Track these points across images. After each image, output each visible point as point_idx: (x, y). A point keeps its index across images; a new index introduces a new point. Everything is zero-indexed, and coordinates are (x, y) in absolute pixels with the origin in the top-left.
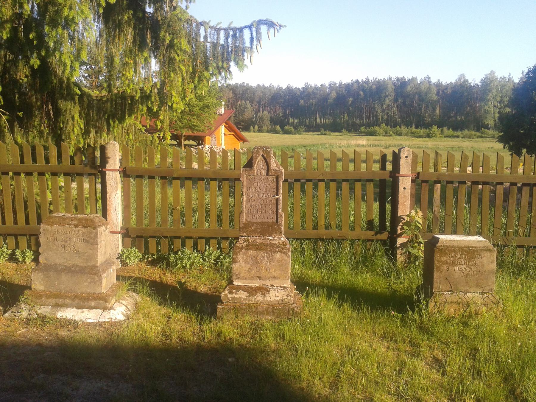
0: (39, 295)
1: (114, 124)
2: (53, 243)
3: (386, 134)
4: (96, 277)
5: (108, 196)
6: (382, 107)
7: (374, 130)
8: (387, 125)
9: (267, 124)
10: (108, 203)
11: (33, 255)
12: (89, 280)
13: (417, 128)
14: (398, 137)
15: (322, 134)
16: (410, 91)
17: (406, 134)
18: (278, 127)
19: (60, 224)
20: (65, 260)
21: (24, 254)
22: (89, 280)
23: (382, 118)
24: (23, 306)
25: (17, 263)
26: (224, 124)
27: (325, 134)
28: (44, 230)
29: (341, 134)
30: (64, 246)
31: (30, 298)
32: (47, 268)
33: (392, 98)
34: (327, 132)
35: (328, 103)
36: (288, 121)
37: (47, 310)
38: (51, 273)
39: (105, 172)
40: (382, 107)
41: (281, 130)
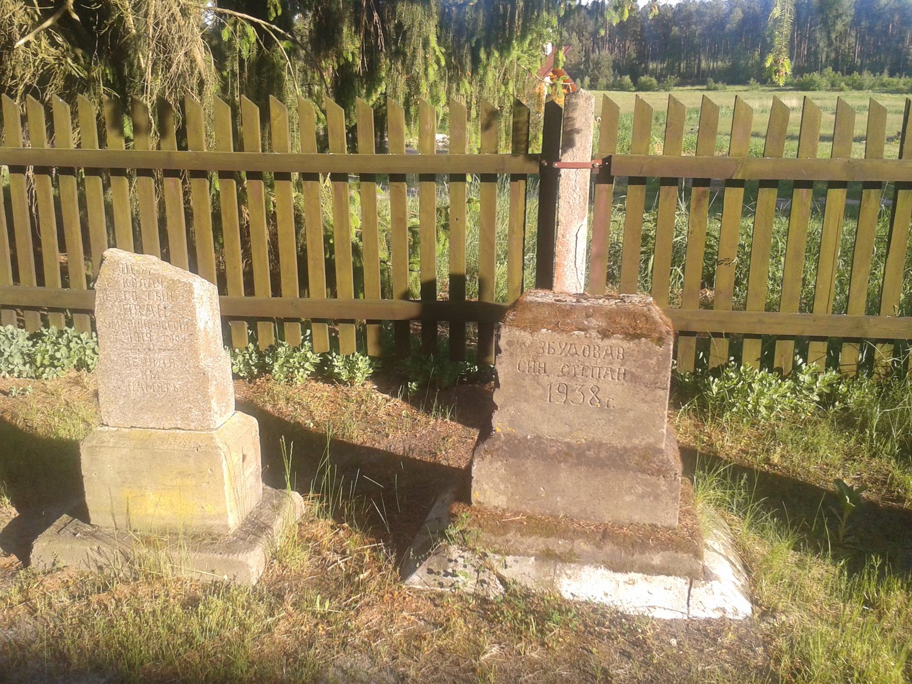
0: (499, 523)
1: (488, 59)
2: (536, 379)
3: (834, 86)
4: (662, 481)
5: (560, 231)
6: (829, 38)
7: (811, 80)
8: (835, 69)
9: (607, 75)
10: (558, 248)
11: (370, 365)
12: (640, 490)
13: (892, 75)
14: (856, 93)
15: (708, 89)
16: (886, 5)
17: (871, 88)
18: (627, 79)
19: (556, 328)
20: (567, 429)
21: (351, 365)
22: (640, 490)
23: (827, 57)
24: (454, 551)
25: (333, 383)
26: (551, 74)
27: (715, 89)
28: (510, 343)
29: (745, 88)
30: (566, 390)
31: (474, 529)
32: (516, 449)
33: (848, 19)
34: (720, 85)
35: (727, 30)
36: (646, 67)
37: (527, 570)
38: (529, 463)
39: (558, 170)
40: (829, 38)
41: (632, 84)
